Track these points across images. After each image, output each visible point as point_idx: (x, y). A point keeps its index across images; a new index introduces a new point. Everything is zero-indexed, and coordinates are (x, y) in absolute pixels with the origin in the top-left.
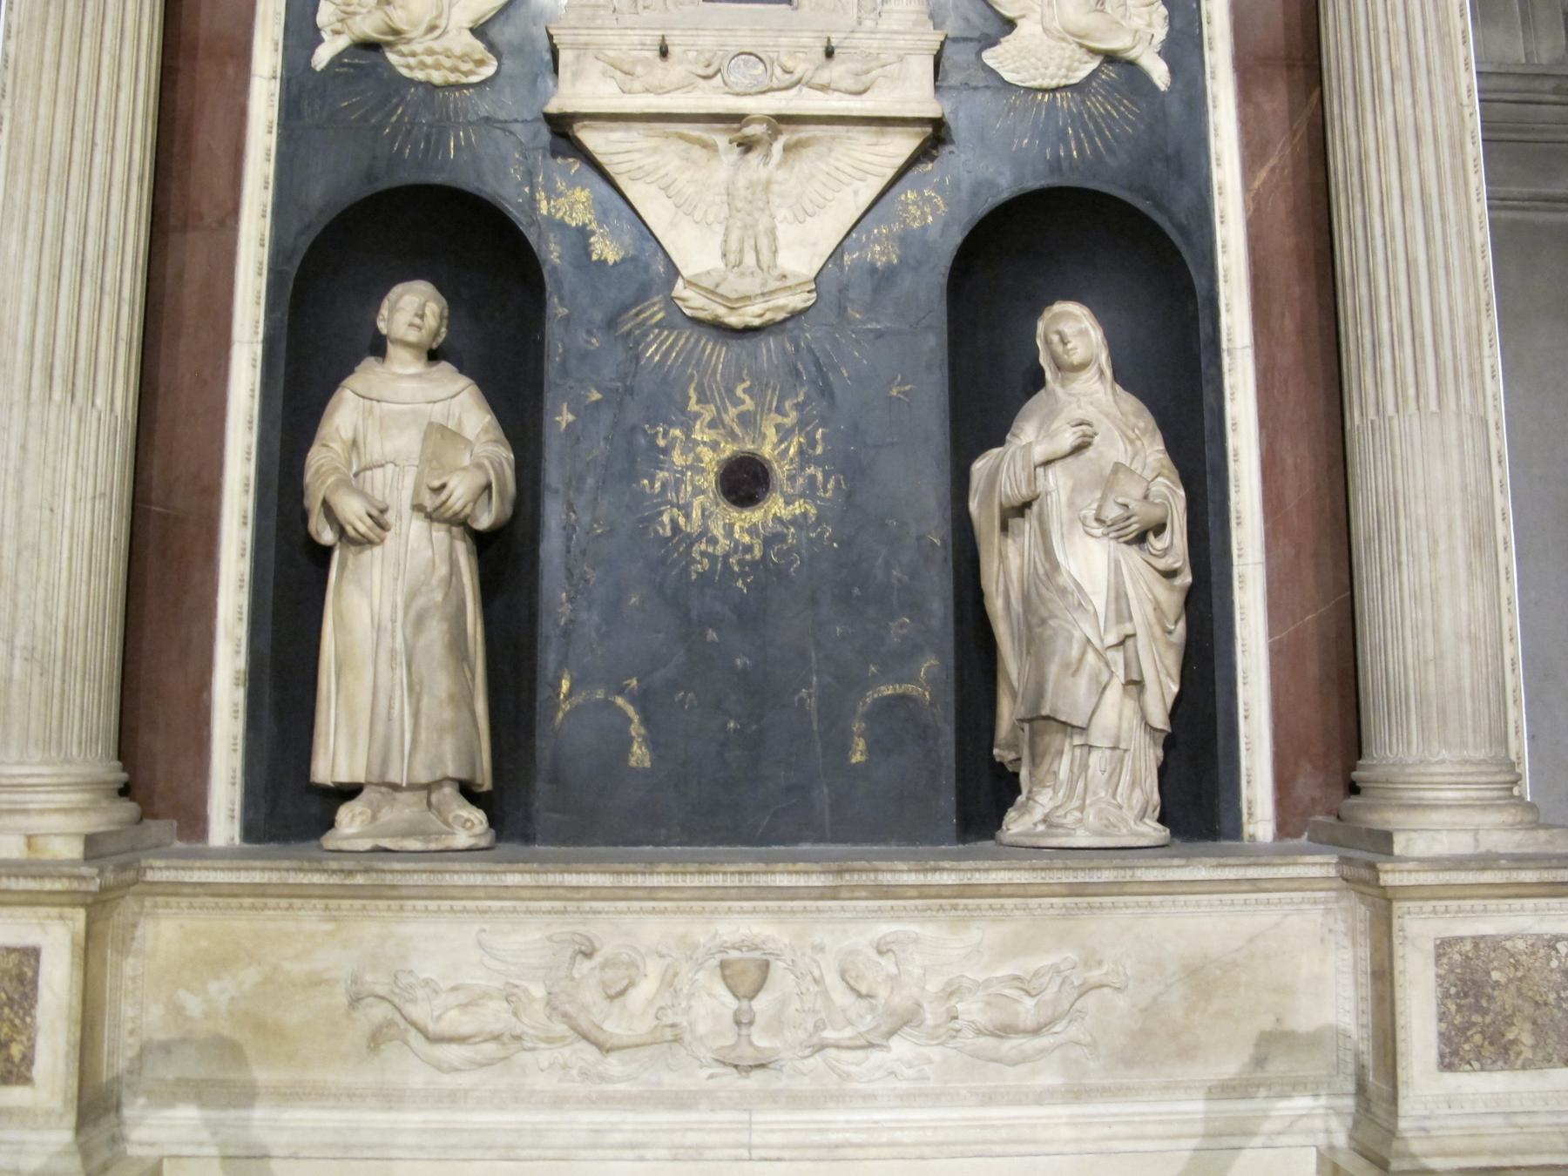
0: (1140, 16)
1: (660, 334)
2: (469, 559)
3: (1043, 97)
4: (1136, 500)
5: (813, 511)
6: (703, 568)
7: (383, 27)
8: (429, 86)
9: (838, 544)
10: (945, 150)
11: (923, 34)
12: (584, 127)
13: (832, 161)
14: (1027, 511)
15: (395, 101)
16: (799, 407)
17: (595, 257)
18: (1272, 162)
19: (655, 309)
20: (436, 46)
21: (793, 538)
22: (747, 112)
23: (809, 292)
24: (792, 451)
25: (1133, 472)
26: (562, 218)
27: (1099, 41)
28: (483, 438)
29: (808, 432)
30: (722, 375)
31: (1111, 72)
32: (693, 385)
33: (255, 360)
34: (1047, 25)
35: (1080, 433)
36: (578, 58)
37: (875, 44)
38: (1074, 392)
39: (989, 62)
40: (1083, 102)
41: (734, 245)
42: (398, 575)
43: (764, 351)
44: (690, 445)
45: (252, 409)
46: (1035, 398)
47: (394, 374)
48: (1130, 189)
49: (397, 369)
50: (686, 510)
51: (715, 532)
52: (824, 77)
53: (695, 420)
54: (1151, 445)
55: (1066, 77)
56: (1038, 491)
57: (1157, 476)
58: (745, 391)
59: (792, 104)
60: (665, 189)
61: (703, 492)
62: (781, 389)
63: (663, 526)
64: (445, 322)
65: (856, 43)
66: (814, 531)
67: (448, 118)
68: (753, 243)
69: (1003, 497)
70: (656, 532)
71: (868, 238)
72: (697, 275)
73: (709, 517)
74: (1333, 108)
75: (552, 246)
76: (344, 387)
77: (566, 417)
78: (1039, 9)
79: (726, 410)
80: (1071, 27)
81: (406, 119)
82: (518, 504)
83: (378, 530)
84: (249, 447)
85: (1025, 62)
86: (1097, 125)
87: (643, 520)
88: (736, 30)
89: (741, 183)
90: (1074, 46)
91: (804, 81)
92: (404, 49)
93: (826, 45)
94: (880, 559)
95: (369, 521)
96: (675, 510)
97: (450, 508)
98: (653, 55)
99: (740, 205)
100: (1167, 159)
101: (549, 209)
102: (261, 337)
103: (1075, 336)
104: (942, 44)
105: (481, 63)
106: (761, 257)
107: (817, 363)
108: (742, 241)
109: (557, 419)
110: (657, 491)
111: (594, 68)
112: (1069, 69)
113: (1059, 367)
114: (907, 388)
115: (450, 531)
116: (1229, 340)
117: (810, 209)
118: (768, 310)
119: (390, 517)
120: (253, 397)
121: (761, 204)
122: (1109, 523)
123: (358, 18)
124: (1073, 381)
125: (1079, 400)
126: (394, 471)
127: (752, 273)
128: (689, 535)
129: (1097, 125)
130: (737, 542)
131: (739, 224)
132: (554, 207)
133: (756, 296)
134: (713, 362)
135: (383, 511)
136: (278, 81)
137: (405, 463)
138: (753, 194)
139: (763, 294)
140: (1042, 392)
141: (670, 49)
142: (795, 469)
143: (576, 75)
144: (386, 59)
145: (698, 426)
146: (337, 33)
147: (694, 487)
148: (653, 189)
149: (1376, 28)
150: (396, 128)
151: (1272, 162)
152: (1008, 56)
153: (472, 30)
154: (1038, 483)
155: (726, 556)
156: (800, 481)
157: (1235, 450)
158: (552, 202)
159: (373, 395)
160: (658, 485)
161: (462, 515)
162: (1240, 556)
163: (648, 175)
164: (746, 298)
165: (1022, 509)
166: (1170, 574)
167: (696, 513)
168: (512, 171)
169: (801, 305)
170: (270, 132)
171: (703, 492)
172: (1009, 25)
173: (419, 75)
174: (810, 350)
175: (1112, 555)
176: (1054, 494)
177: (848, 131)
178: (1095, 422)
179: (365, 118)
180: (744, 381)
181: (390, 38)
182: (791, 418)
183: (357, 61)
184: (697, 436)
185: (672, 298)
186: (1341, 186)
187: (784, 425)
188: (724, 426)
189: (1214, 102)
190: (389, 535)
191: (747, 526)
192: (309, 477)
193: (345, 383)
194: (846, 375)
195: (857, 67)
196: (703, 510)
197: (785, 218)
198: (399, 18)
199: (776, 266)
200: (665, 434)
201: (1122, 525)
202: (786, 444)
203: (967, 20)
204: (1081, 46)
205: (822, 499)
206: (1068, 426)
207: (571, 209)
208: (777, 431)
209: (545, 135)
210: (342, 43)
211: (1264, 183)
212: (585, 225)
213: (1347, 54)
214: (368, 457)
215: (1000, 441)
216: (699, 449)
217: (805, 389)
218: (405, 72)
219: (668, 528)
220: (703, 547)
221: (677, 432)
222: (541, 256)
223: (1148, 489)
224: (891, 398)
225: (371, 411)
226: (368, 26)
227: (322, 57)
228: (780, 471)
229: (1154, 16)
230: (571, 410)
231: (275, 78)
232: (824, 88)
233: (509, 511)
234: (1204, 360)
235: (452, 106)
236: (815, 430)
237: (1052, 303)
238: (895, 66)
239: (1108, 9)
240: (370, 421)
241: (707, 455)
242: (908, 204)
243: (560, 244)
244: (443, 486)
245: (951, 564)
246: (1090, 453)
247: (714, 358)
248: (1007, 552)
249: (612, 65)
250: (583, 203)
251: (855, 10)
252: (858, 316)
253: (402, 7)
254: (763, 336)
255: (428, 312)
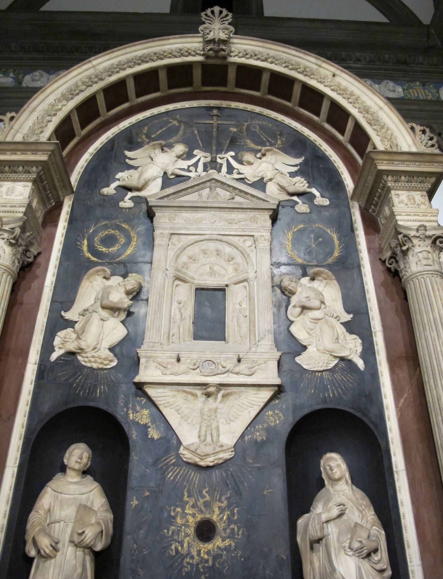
0: (351, 343)
1: (174, 468)
2: (91, 563)
3: (318, 374)
4: (365, 539)
5: (233, 544)
6: (188, 570)
7: (77, 347)
8: (91, 368)
9: (244, 559)
10: (283, 395)
11: (273, 353)
12: (148, 387)
13: (240, 400)
14: (321, 541)
15: (79, 374)
16: (227, 499)
17: (149, 437)
18: (405, 396)
19: (172, 458)
20: (96, 355)
21: (225, 556)
22: (208, 382)
23: (232, 452)
24: (225, 518)
25: (362, 526)
26: (138, 421)
27: (338, 353)
28: (101, 509)
29: (231, 510)
30: (198, 486)
31: (343, 364)
32: (186, 490)
33: (13, 474)
34: (319, 348)
35: (340, 510)
36: (147, 362)
37: (256, 357)
38: (336, 490)
39: (298, 361)
40: (333, 375)
41: (203, 433)
42: (60, 573)
43: (214, 475)
44: (184, 515)
45: (9, 495)
46: (321, 491)
47: (68, 482)
48: (353, 408)
49: (70, 480)
50: (181, 543)
51: (193, 554)
52: (237, 369)
53: (187, 504)
54: (369, 512)
55: (326, 366)
56: (325, 534)
57: (373, 526)
58: (206, 492)
59: (225, 380)
60: (177, 411)
61: (189, 536)
62: (220, 492)
63: (172, 551)
64: (90, 459)
65: (249, 356)
66: (233, 553)
67: (98, 381)
68: (210, 432)
69: (311, 536)
70: (169, 553)
71: (254, 430)
72: (189, 445)
73: (191, 547)
74: (426, 378)
75: (134, 432)
76: (48, 486)
77: (135, 502)
78: (315, 342)
79: (199, 500)
80: (328, 349)
81: (82, 381)
82: (113, 538)
83: (54, 552)
84: (6, 512)
85: (311, 362)
86: (339, 384)
87: (164, 548)
88: (205, 352)
89: (206, 409)
90: (328, 355)
91: (230, 371)
92: (84, 355)
93: (237, 357)
94: (261, 566)
95: (51, 548)
96: (177, 543)
97: (85, 542)
98: (174, 361)
99: (205, 417)
100: (366, 396)
101: (133, 418)
102: (17, 464)
103: (335, 467)
104: (280, 356)
105: (111, 361)
106: (213, 438)
107: (235, 481)
108: (206, 431)
109: (132, 503)
110: (170, 535)
111: (153, 365)
112: (327, 363)
113: (330, 478)
114: (270, 491)
115: (84, 551)
116: (396, 467)
117: (232, 419)
118: (216, 459)
119: (60, 546)
120: (10, 490)
121: (213, 417)
122: (355, 550)
123: (68, 343)
124: (336, 485)
125: (339, 494)
126: (64, 524)
127: (210, 444)
128: (183, 555)
129: (339, 384)
130: (202, 558)
131: (205, 425)
132: (135, 416)
133: (211, 454)
134: (194, 480)
135: (57, 543)
136: (37, 365)
137: (69, 521)
138: (210, 414)
139: (214, 453)
140: (324, 489)
141: (181, 358)
142: (226, 526)
143: (146, 367)
144: (77, 358)
145: (187, 507)
146: (60, 348)
147: (185, 533)
148: (173, 411)
149: (437, 350)
150: (78, 385)
151: (405, 396)
152: (304, 359)
153: (109, 349)
154: (325, 530)
155: (197, 564)
156: (228, 531)
157: (403, 514)
158: (134, 415)
159: (59, 491)
160: (170, 532)
161: (90, 545)
162: (411, 562)
163: (171, 405)
164: (207, 455)
165: (319, 541)
166: (382, 571)
167: (185, 545)
168: (120, 402)
169: (229, 457)
170: (31, 384)
171: (189, 536)
172: (305, 348)
173: (89, 365)
174: (232, 475)
175: (357, 563)
176: (331, 535)
177: (246, 389)
178: (346, 503)
179: (67, 380)
180: (206, 488)
181: (79, 351)
182: (225, 504)
183: (66, 358)
184: (187, 511)
185: (179, 454)
186: (432, 408)
187: (222, 506)
188: (198, 507)
189: (381, 374)
190: (59, 554)
191: (206, 551)
192: (28, 526)
193: (48, 484)
194: (246, 485)
195: (250, 365)
196: (189, 543)
197: (223, 422)
198: (83, 344)
199: (219, 442)
200: (174, 510)
201: (360, 551)
202: (222, 515)
203: (289, 346)
204: (331, 355)
205: (237, 539)
206: (335, 506)
207: (142, 417)
208: (219, 509)
209: (134, 389)
210: (62, 352)
211: (403, 404)
212: (146, 424)
213: (428, 359)
214: (54, 518)
215: (307, 511)
216: (188, 517)
217: (230, 491)
218: (83, 363)
219: (174, 551)
220: (188, 560)
221: (179, 509)
222: (129, 436)
223: (370, 532)
224: (264, 495)
225: (57, 497)
226: (71, 347)
227: (54, 356)
228: (220, 526)
229: (357, 343)
230: (137, 500)
231: (36, 364)
232: (237, 373)
233: (109, 541)
234: (387, 476)
235: (99, 376)
236: (234, 509)
237: (326, 453)
238: (263, 365)
239: (340, 342)
240: (56, 503)
241: (191, 519)
242: (269, 416)
243: (137, 431)
244: (83, 532)
245: (290, 568)
246: (345, 517)
247: (194, 478)
248: (313, 559)
249: (159, 364)
250: (146, 415)
251: (249, 344)
252: (251, 461)
253: (84, 341)
254: (213, 470)
255: (84, 456)
